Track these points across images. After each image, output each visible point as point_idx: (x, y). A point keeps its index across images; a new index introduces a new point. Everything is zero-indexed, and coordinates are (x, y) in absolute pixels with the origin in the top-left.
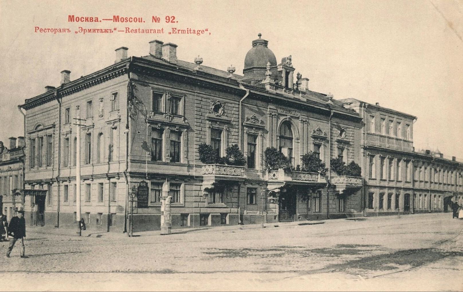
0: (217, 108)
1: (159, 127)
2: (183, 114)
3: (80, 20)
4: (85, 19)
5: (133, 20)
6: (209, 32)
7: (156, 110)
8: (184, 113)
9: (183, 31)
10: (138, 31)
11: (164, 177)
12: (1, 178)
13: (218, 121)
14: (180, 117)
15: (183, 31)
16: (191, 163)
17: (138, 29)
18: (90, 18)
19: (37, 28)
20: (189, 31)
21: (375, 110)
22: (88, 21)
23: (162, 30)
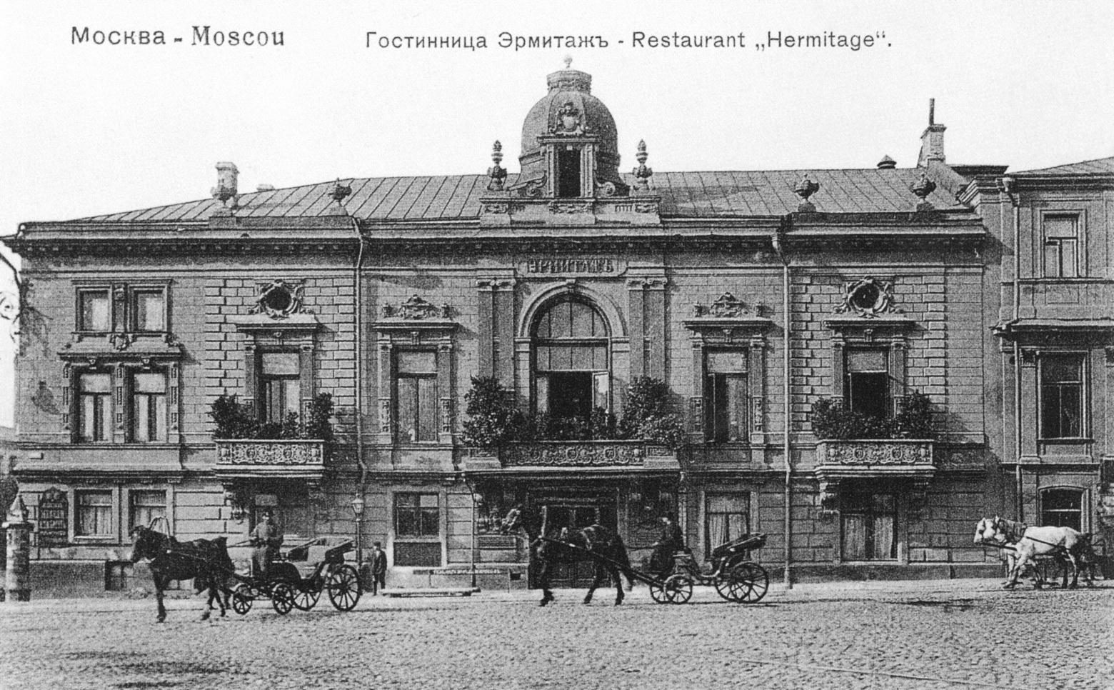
0: (865, 296)
1: (145, 365)
2: (166, 327)
3: (107, 39)
4: (122, 37)
5: (255, 38)
6: (887, 40)
7: (83, 329)
8: (170, 324)
9: (811, 40)
10: (672, 41)
11: (107, 479)
12: (451, 689)
13: (413, 330)
14: (157, 334)
15: (811, 40)
16: (189, 441)
17: (671, 35)
18: (141, 33)
19: (279, 39)
20: (828, 40)
21: (757, 256)
22: (133, 42)
23: (741, 36)
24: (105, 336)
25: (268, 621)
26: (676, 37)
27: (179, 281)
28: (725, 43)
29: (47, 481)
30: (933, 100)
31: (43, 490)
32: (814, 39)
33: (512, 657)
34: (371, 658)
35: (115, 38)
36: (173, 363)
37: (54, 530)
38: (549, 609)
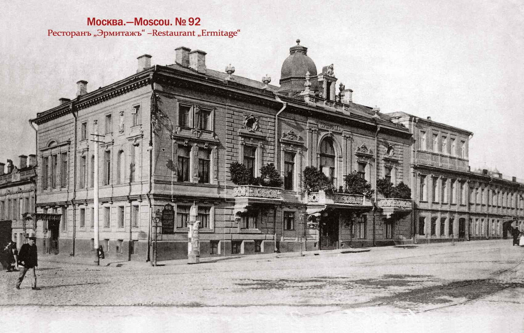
0: (250, 123)
1: (185, 144)
4: (106, 22)
14: (210, 132)
16: (221, 184)
19: (50, 32)
23: (193, 32)
24: (211, 133)
25: (111, 259)
26: (167, 32)
27: (217, 108)
28: (187, 34)
29: (166, 200)
30: (138, 58)
31: (165, 205)
32: (214, 32)
33: (109, 268)
34: (144, 284)
35: (104, 23)
36: (196, 144)
37: (168, 225)
38: (333, 291)
